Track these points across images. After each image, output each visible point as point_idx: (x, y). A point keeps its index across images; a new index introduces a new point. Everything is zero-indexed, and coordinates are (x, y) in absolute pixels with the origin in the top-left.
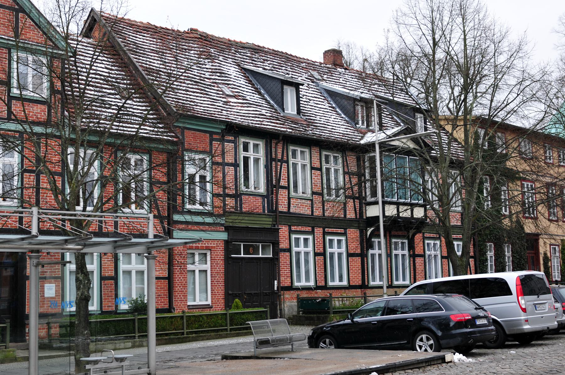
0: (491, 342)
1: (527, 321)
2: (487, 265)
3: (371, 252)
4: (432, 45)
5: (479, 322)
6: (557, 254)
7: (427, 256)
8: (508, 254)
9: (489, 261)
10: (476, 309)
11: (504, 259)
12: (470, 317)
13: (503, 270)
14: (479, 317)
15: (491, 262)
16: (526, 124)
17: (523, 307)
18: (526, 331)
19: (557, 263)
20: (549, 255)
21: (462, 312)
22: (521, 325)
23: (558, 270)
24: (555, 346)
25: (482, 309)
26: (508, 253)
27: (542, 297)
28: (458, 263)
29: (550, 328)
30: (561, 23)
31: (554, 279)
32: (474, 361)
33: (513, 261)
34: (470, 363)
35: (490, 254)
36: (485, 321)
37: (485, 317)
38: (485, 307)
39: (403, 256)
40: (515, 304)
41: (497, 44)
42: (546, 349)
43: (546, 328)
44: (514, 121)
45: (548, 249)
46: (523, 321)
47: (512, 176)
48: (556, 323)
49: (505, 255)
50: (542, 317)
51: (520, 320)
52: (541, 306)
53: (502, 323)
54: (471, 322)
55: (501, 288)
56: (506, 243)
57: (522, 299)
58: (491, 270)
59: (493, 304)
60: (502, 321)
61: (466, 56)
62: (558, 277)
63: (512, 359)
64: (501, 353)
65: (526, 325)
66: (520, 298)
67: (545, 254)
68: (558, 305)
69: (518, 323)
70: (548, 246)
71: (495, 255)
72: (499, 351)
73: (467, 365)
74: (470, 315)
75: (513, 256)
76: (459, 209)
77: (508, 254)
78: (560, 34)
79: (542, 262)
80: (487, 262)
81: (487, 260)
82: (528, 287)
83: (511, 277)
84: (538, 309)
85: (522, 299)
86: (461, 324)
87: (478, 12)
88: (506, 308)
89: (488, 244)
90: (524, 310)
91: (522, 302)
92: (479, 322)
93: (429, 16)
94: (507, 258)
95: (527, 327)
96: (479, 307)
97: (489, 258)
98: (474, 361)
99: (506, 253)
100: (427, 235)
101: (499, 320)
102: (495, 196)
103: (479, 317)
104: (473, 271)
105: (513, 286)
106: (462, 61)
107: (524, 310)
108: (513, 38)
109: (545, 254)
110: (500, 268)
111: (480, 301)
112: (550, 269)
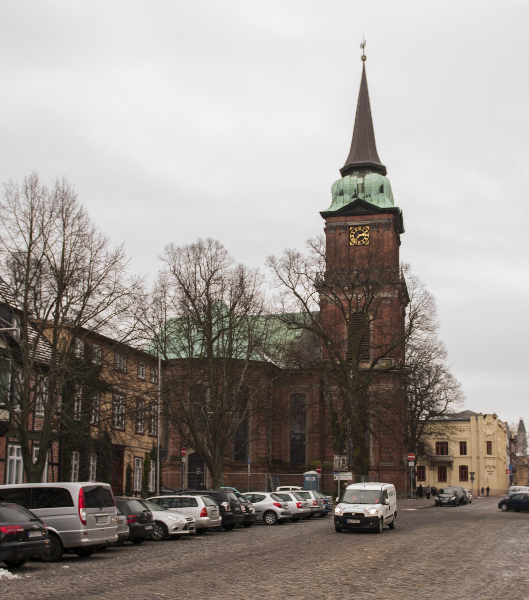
0: (47, 555)
1: (86, 534)
2: (71, 473)
3: (10, 457)
4: (28, 243)
5: (32, 535)
6: (140, 466)
7: (8, 461)
8: (93, 463)
9: (73, 469)
10: (31, 520)
11: (89, 468)
12: (22, 530)
13: (67, 479)
14: (33, 530)
15: (75, 470)
16: (114, 336)
17: (84, 519)
18: (84, 545)
19: (140, 474)
20: (132, 466)
21: (14, 524)
22: (80, 538)
23: (139, 481)
24: (112, 560)
25: (39, 520)
26: (93, 462)
27: (104, 509)
28: (33, 469)
29: (110, 541)
30: (166, 252)
31: (135, 490)
32: (20, 577)
33: (97, 471)
34: (14, 580)
35: (75, 462)
36: (39, 534)
37: (41, 529)
38: (42, 519)
39: (18, 462)
40: (75, 516)
41: (95, 252)
42: (102, 563)
43: (105, 542)
44: (106, 332)
45: (133, 460)
46: (82, 534)
47: (105, 387)
48: (117, 536)
49: (89, 465)
50: (103, 530)
51: (79, 533)
52: (103, 519)
53: (60, 536)
54: (24, 535)
55: (62, 498)
56: (92, 453)
57: (83, 511)
58: (75, 478)
59: (52, 516)
60: (61, 533)
61: (63, 260)
62: (139, 488)
63: (64, 577)
64: (54, 569)
65: (84, 538)
66: (81, 510)
67: (129, 465)
68: (123, 517)
69: (77, 536)
70: (133, 458)
71: (80, 464)
72: (53, 565)
73: (8, 582)
74: (22, 527)
75: (97, 466)
76: (43, 414)
77: (93, 463)
78: (165, 263)
79: (125, 473)
80: (72, 470)
81: (71, 468)
82: (90, 499)
83: (75, 488)
84: (99, 522)
85: (83, 511)
86: (13, 536)
87: (79, 217)
88: (72, 520)
89: (74, 453)
90: (84, 523)
91: (83, 514)
92: (32, 535)
93: (28, 213)
94: (91, 468)
95: (85, 540)
96: (36, 519)
97: (73, 467)
98: (20, 577)
99: (91, 463)
100: (11, 439)
101: (57, 532)
102: (87, 407)
103: (33, 530)
104: (55, 479)
105: (75, 497)
106: (59, 264)
107: (84, 523)
108: (110, 249)
109: (129, 465)
110: (64, 477)
111: (38, 511)
112: (132, 480)
